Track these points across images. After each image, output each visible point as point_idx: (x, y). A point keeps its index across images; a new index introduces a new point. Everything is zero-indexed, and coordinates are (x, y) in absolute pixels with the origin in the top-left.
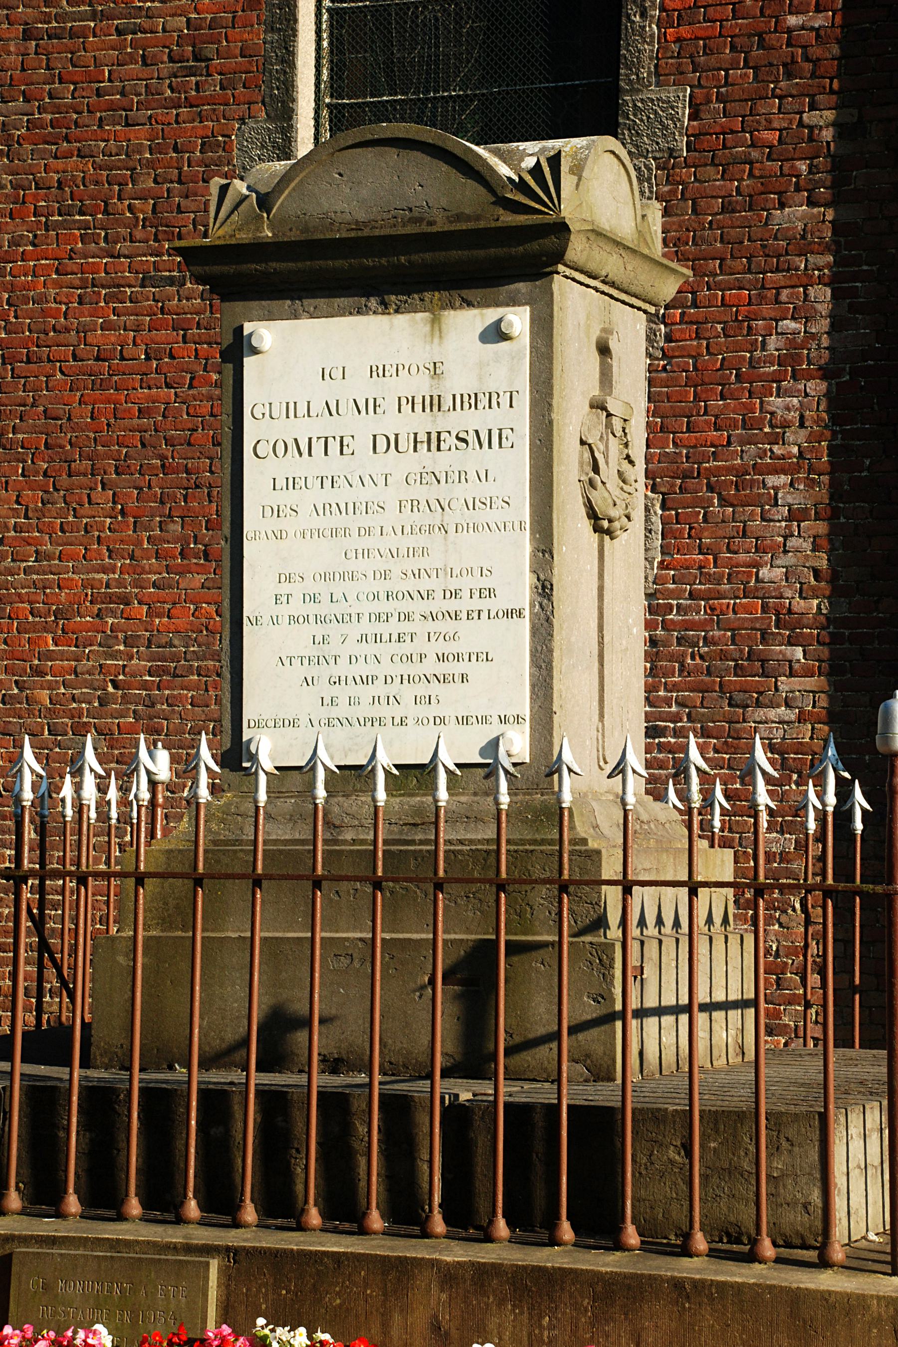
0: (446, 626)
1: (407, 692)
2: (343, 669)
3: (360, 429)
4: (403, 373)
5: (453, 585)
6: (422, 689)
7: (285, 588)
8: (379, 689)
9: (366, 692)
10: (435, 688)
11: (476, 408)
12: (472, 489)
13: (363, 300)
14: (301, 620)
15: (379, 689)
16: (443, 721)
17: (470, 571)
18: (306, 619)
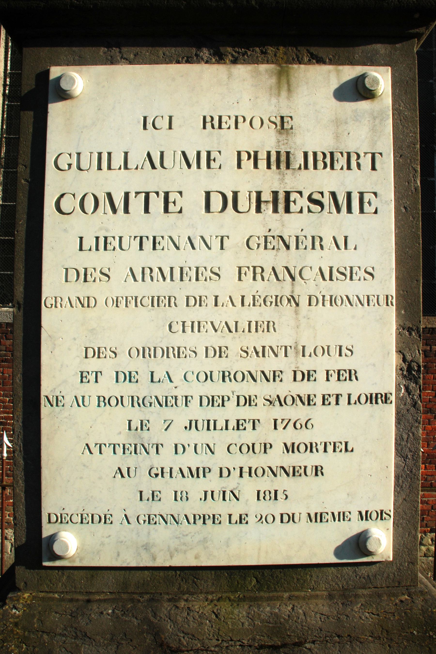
0: (299, 412)
1: (248, 487)
2: (166, 459)
3: (192, 184)
4: (244, 126)
5: (306, 364)
6: (266, 483)
7: (93, 364)
8: (213, 483)
9: (196, 487)
10: (283, 483)
11: (332, 168)
12: (329, 258)
13: (194, 50)
14: (113, 402)
15: (213, 483)
16: (292, 518)
17: (326, 351)
18: (120, 401)
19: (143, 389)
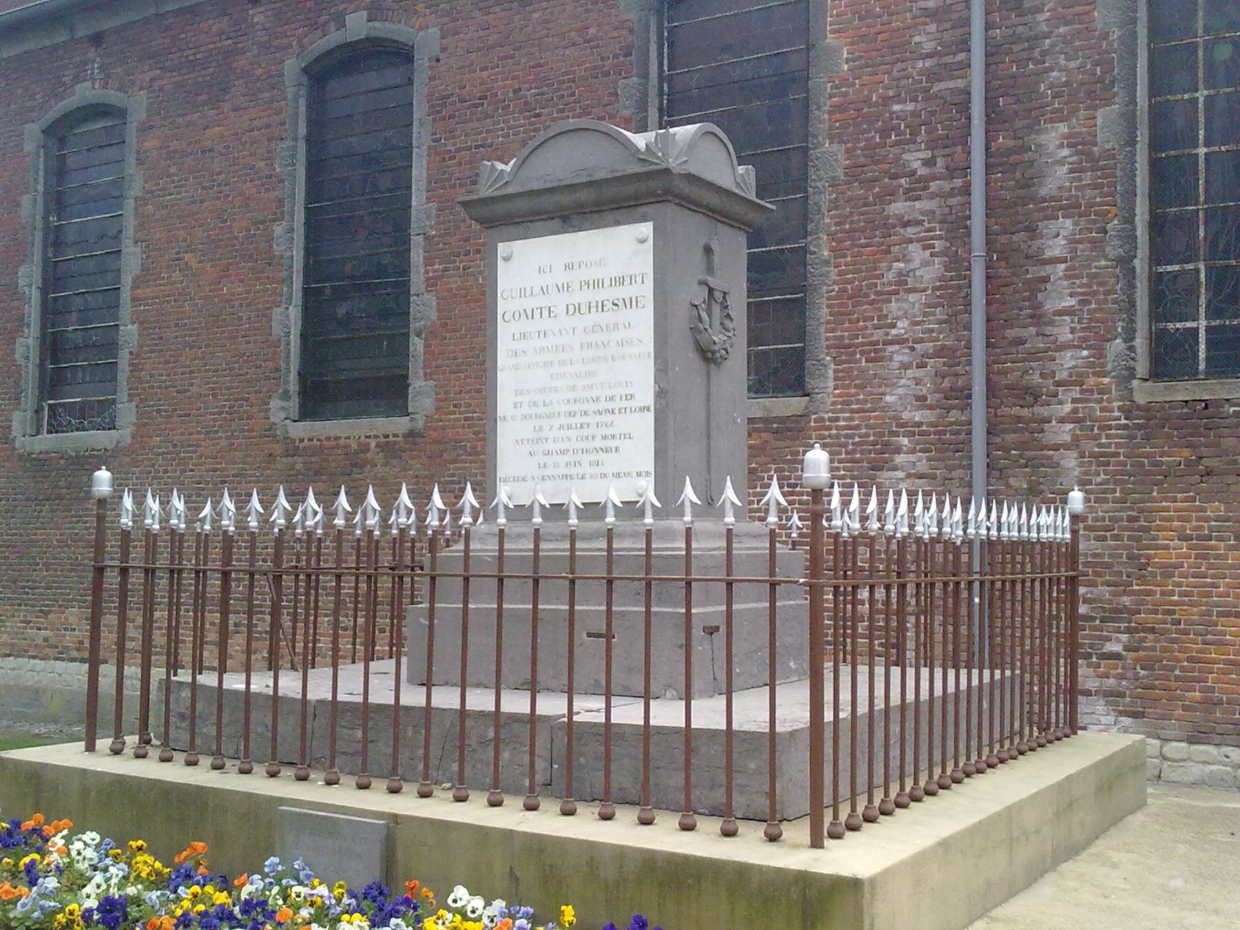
0: (607, 418)
1: (586, 459)
2: (550, 446)
3: (559, 301)
6: (593, 457)
7: (520, 399)
8: (570, 457)
10: (602, 456)
15: (570, 457)
19: (541, 410)
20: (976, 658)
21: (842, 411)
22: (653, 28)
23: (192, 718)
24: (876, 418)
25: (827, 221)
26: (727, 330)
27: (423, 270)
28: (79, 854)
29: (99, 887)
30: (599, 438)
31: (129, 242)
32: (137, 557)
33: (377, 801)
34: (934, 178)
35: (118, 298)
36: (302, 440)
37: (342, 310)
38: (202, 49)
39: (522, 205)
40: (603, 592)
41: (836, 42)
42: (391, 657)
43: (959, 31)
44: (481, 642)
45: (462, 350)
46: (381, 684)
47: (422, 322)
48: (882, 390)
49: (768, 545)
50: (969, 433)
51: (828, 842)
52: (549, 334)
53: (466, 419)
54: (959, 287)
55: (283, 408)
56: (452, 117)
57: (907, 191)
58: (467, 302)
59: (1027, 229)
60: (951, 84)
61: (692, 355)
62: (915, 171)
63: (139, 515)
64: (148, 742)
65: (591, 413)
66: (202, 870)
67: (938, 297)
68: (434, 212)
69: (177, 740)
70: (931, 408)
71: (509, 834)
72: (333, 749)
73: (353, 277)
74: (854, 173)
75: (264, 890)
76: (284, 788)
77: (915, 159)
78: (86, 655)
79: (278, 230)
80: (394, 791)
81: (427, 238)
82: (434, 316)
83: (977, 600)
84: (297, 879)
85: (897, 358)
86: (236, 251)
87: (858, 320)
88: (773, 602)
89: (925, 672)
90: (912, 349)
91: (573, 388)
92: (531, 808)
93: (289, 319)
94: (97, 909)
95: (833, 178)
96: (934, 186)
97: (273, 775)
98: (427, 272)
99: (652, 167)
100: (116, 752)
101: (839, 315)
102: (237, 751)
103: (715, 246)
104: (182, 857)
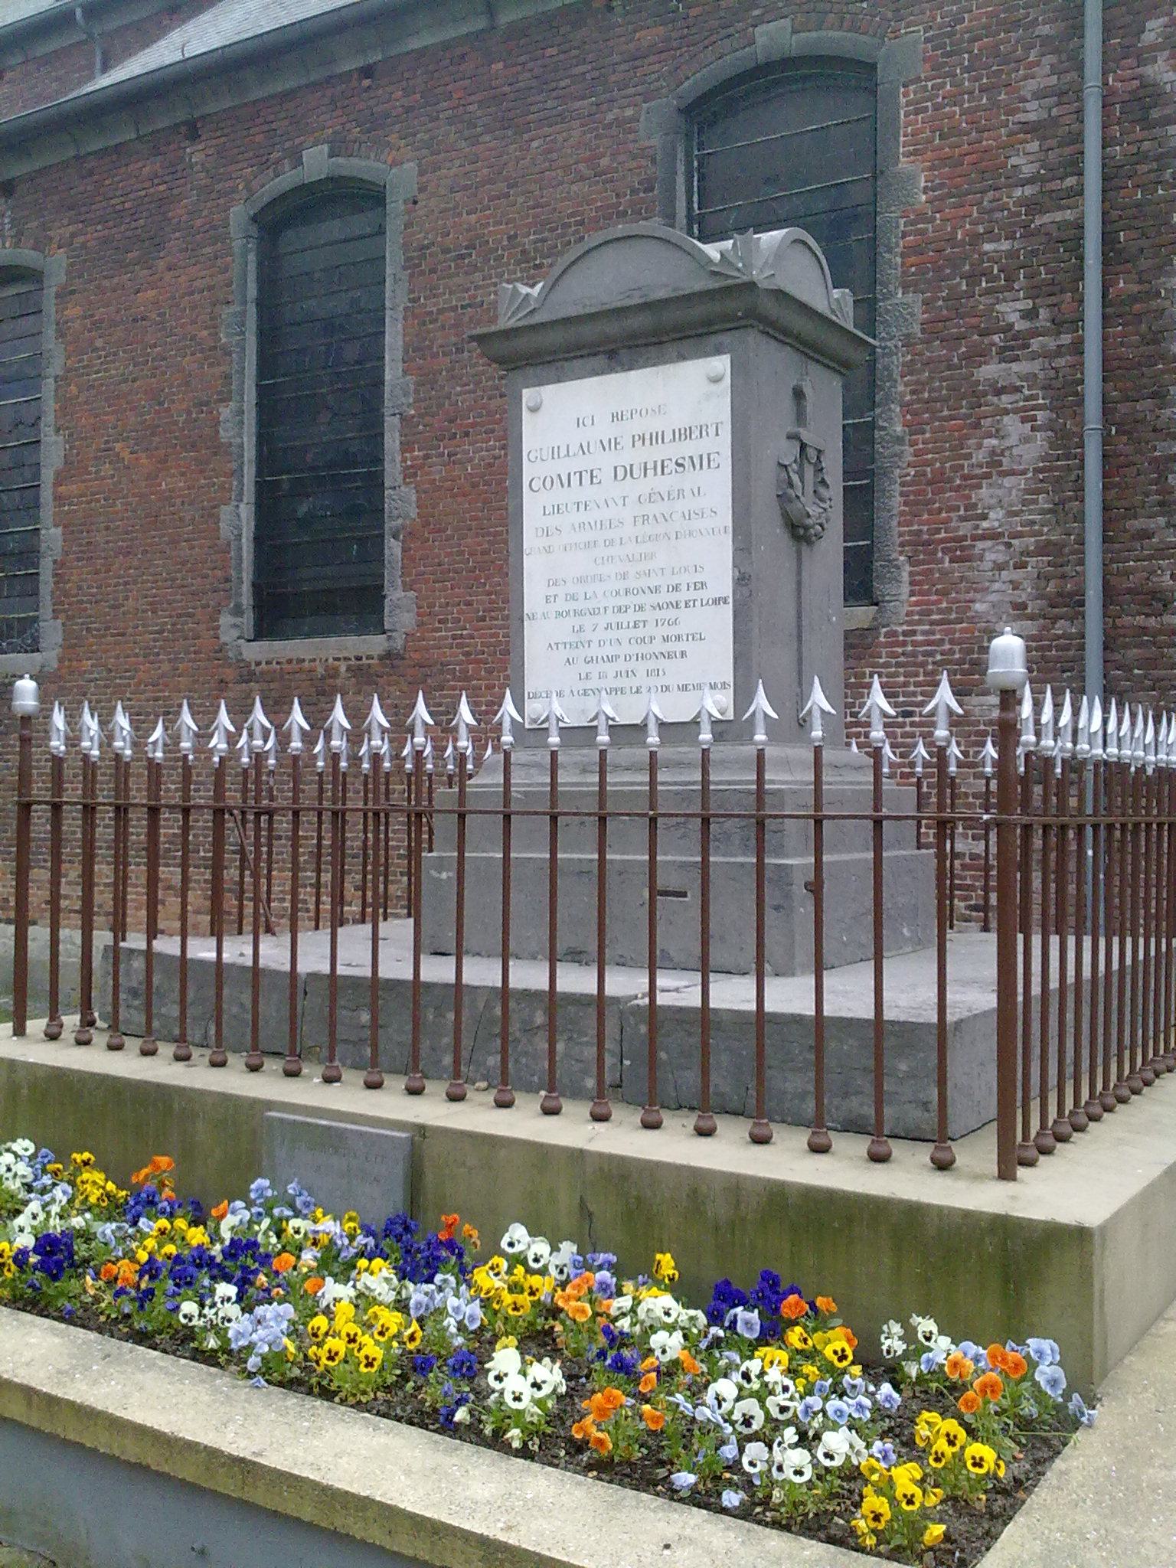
0: (671, 614)
1: (641, 667)
2: (594, 651)
6: (652, 664)
7: (553, 591)
8: (621, 665)
9: (610, 669)
10: (663, 663)
15: (621, 665)
20: (1089, 924)
21: (919, 623)
22: (681, 156)
23: (148, 994)
24: (962, 630)
25: (901, 388)
26: (822, 500)
27: (399, 458)
28: (9, 1170)
29: (35, 1217)
30: (659, 639)
31: (50, 430)
32: (73, 792)
33: (392, 1105)
34: (1034, 333)
35: (37, 498)
36: (258, 664)
37: (303, 509)
38: (132, 196)
39: (556, 337)
40: (677, 834)
41: (911, 168)
42: (363, 921)
43: (1067, 150)
44: (528, 900)
45: (448, 555)
46: (388, 951)
47: (400, 521)
48: (971, 595)
49: (872, 779)
50: (1082, 647)
51: (1021, 1172)
52: (591, 505)
53: (454, 637)
54: (1069, 468)
55: (235, 626)
56: (433, 271)
57: (1002, 350)
58: (453, 496)
59: (1154, 395)
60: (1058, 216)
61: (780, 532)
62: (1011, 326)
63: (73, 741)
64: (92, 1023)
65: (648, 607)
66: (167, 1192)
67: (1041, 481)
68: (412, 387)
69: (128, 1022)
70: (1032, 617)
71: (578, 1156)
72: (332, 1034)
73: (313, 469)
74: (933, 329)
75: (250, 1222)
76: (267, 1086)
77: (1011, 311)
78: (12, 915)
79: (225, 412)
80: (414, 1092)
81: (404, 419)
82: (413, 513)
83: (1090, 853)
84: (292, 1206)
85: (990, 556)
86: (176, 438)
87: (940, 510)
88: (878, 849)
89: (1054, 940)
90: (1009, 545)
91: (624, 576)
92: (599, 1118)
93: (239, 519)
94: (35, 1250)
95: (908, 336)
96: (1035, 343)
97: (254, 1069)
98: (404, 460)
99: (730, 282)
100: (52, 1037)
101: (916, 505)
102: (206, 1037)
103: (808, 391)
104: (141, 1177)
